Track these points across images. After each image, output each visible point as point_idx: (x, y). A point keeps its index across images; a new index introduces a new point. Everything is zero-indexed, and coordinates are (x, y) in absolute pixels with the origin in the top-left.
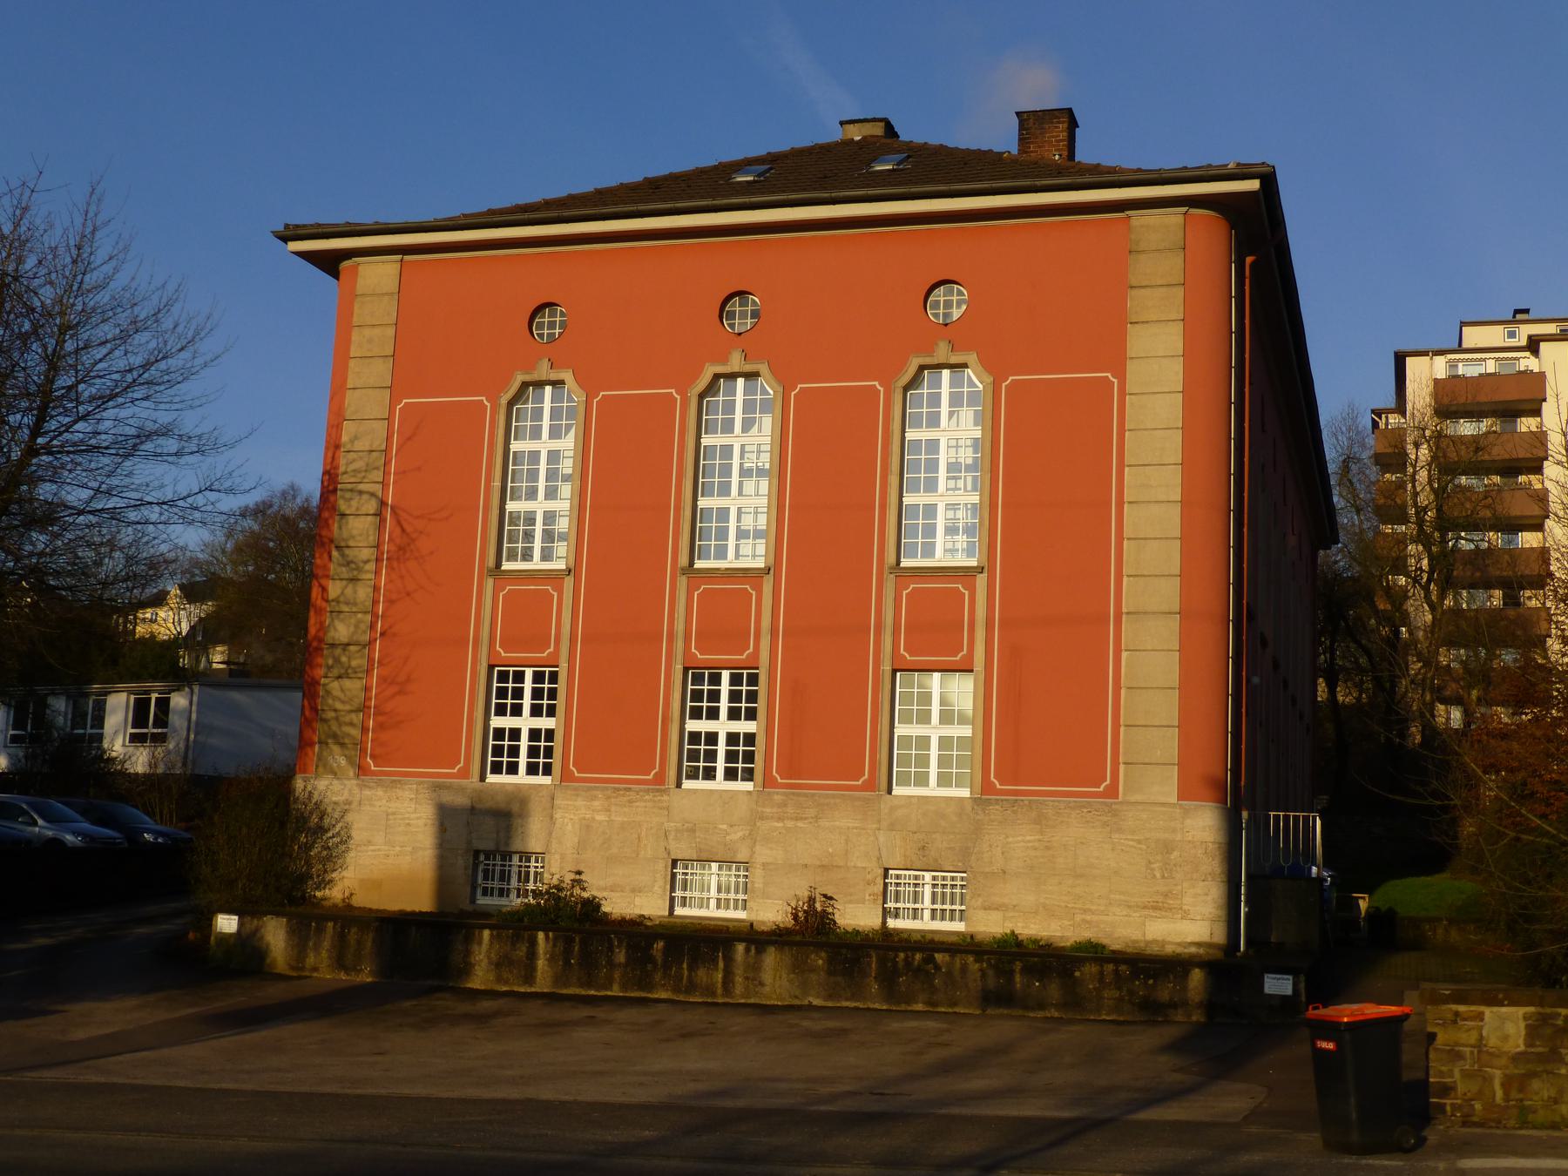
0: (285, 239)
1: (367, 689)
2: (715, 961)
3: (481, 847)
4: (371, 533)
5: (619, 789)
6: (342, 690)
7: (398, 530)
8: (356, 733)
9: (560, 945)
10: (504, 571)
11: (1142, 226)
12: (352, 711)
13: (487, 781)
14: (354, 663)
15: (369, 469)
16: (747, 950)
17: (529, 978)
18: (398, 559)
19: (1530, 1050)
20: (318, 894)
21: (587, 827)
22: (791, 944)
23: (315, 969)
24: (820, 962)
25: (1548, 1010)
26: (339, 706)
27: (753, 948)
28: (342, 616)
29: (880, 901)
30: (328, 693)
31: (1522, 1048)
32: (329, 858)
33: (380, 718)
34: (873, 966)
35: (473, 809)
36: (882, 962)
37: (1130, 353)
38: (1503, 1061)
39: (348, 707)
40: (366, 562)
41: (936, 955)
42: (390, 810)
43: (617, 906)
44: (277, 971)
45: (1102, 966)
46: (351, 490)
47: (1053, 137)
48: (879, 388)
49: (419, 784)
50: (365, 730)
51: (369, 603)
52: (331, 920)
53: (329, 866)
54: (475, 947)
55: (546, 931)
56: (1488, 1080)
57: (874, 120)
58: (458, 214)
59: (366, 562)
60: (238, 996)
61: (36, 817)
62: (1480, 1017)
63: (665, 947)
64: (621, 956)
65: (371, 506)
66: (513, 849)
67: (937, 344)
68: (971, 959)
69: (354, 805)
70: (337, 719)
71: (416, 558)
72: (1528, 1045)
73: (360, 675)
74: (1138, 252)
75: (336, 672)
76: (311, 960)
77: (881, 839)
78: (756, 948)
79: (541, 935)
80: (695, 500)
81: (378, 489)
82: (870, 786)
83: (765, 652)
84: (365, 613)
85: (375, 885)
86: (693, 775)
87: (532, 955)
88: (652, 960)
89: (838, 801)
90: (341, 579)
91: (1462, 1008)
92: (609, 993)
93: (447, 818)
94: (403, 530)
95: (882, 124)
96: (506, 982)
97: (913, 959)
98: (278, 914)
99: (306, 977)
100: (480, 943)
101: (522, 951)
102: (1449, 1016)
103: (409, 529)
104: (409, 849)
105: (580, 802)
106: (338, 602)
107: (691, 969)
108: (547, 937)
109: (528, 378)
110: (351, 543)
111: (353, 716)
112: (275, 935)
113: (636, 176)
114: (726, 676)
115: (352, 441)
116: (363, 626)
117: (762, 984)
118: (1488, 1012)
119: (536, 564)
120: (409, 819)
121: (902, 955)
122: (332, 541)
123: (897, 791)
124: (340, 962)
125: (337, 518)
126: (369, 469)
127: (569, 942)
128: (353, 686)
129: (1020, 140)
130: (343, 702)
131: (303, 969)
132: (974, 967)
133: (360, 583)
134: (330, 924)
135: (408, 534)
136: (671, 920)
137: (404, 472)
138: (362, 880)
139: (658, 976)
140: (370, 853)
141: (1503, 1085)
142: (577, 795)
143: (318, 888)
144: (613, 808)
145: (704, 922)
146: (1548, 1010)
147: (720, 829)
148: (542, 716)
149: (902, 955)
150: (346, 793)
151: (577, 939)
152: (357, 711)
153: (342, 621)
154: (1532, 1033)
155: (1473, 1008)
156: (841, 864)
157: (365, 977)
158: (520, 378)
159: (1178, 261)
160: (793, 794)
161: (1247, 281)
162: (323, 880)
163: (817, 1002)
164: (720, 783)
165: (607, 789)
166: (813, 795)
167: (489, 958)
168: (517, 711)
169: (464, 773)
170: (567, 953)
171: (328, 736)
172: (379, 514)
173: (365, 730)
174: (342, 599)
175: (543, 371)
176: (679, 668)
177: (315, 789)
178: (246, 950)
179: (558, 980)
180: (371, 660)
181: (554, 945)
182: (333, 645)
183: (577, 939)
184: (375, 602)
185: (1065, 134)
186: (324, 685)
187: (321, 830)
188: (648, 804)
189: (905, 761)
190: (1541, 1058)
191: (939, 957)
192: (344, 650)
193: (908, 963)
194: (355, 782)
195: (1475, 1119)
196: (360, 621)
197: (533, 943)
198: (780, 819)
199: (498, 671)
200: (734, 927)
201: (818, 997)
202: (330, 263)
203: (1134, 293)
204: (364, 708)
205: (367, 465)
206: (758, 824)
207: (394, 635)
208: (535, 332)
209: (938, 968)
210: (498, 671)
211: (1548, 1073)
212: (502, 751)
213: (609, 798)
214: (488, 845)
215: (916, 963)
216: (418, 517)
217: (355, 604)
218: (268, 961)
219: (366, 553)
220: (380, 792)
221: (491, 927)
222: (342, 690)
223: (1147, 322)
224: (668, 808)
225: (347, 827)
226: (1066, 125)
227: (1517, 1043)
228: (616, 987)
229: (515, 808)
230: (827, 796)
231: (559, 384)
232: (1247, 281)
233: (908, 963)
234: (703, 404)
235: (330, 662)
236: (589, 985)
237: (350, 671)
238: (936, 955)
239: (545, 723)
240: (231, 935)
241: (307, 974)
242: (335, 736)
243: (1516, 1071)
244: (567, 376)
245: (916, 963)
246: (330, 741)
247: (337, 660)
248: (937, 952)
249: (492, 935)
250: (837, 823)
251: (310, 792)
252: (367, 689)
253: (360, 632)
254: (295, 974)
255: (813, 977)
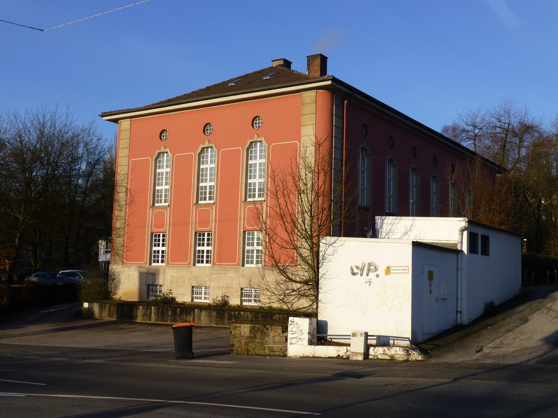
0: (103, 117)
1: (124, 240)
2: (191, 314)
3: (149, 283)
4: (125, 197)
5: (180, 267)
6: (119, 241)
7: (131, 196)
8: (121, 252)
9: (157, 310)
10: (156, 206)
11: (305, 96)
12: (121, 247)
13: (152, 265)
14: (121, 233)
15: (124, 179)
16: (198, 311)
17: (150, 319)
18: (131, 204)
19: (250, 335)
20: (114, 297)
21: (173, 277)
22: (207, 309)
23: (104, 317)
24: (215, 314)
25: (254, 325)
26: (118, 245)
27: (199, 310)
28: (118, 220)
29: (240, 297)
30: (115, 242)
31: (248, 335)
32: (116, 287)
33: (127, 248)
34: (227, 315)
35: (147, 273)
36: (228, 314)
37: (302, 135)
38: (244, 338)
39: (120, 246)
40: (124, 205)
41: (241, 312)
42: (129, 274)
43: (179, 300)
44: (96, 318)
45: (280, 315)
46: (120, 185)
47: (316, 63)
48: (241, 149)
49: (136, 266)
50: (123, 252)
51: (124, 217)
52: (108, 304)
53: (116, 289)
54: (138, 311)
55: (154, 306)
56: (241, 342)
57: (281, 59)
58: (118, 110)
59: (124, 205)
60: (88, 322)
61: (81, 276)
62: (240, 327)
63: (180, 311)
64: (170, 313)
65: (124, 190)
66: (158, 284)
67: (254, 135)
68: (249, 313)
69: (121, 273)
70: (117, 249)
71: (135, 204)
72: (250, 334)
73: (122, 237)
74: (304, 104)
75: (117, 236)
76: (103, 315)
77: (240, 279)
78: (200, 311)
79: (153, 307)
80: (246, 180)
81: (126, 185)
82: (238, 265)
83: (213, 226)
84: (124, 219)
85: (126, 294)
86: (198, 262)
87: (151, 313)
88: (176, 314)
89: (230, 269)
90: (118, 210)
91: (237, 325)
92: (168, 323)
93: (142, 276)
94: (132, 196)
95: (283, 60)
96: (145, 320)
97: (236, 313)
98: (96, 302)
99: (102, 319)
100: (139, 310)
101: (148, 312)
102: (234, 327)
103: (133, 196)
104: (133, 284)
105: (171, 270)
106: (117, 217)
107: (186, 316)
108: (154, 308)
109: (159, 151)
110: (120, 200)
111: (121, 248)
112: (96, 308)
113: (204, 86)
114: (206, 234)
115: (120, 172)
116: (123, 223)
117: (201, 321)
118: (242, 325)
119: (208, 201)
120: (133, 276)
121: (233, 312)
122: (116, 200)
123: (246, 265)
124: (110, 315)
125: (117, 193)
126: (124, 179)
127: (159, 309)
128: (121, 239)
129: (308, 65)
130: (119, 244)
131: (101, 317)
132: (250, 316)
133: (122, 211)
134: (108, 305)
135: (133, 197)
136: (192, 303)
137: (132, 180)
138: (123, 293)
139: (178, 319)
140: (125, 285)
141: (244, 344)
142: (170, 269)
143: (114, 295)
144: (179, 272)
145: (198, 304)
146: (254, 325)
147: (203, 277)
148: (209, 246)
149: (233, 312)
150: (120, 269)
151: (161, 308)
152: (122, 246)
153: (118, 222)
154: (251, 331)
155: (239, 325)
156: (231, 287)
157: (114, 319)
158: (249, 141)
159: (314, 106)
160: (220, 267)
161: (345, 108)
162: (115, 293)
163: (214, 325)
164: (205, 264)
165: (177, 267)
166: (224, 267)
167: (141, 314)
168: (203, 245)
169: (146, 263)
170: (158, 312)
171: (116, 254)
172: (126, 192)
173: (123, 252)
174: (118, 216)
175: (163, 150)
176: (194, 232)
177: (113, 268)
178: (90, 311)
179: (157, 319)
180: (125, 232)
181: (156, 310)
182: (116, 229)
183: (161, 308)
184: (126, 216)
185: (320, 62)
186: (115, 240)
187: (114, 279)
188: (187, 271)
189: (248, 257)
190: (252, 338)
191: (241, 313)
192: (119, 230)
193: (234, 314)
194: (121, 266)
195: (239, 353)
196: (122, 222)
197: (151, 309)
198: (217, 274)
199: (155, 234)
200: (205, 305)
201: (214, 324)
202: (116, 121)
203: (303, 116)
204: (123, 245)
205: (124, 178)
206: (212, 276)
207: (130, 225)
208: (254, 126)
209: (241, 316)
210: (155, 234)
211: (253, 341)
212: (154, 256)
213: (178, 269)
214: (150, 283)
215: (236, 315)
216: (135, 192)
217: (121, 217)
218: (95, 315)
219: (123, 203)
220: (127, 269)
221: (142, 305)
222: (119, 241)
223: (306, 125)
224: (191, 272)
225: (120, 279)
226: (320, 59)
227: (247, 334)
228: (169, 321)
229: (157, 272)
230: (228, 268)
231: (211, 147)
232: (345, 108)
233: (234, 314)
234: (249, 151)
235: (116, 233)
236: (163, 321)
237: (120, 236)
238: (241, 312)
239: (210, 248)
240: (87, 308)
241: (102, 318)
242: (117, 254)
243: (247, 341)
244: (263, 139)
245: (236, 315)
246: (116, 255)
247: (117, 233)
248: (241, 311)
249: (142, 307)
250: (230, 275)
251: (112, 269)
252: (124, 240)
253: (122, 225)
254: (100, 318)
255: (213, 318)
